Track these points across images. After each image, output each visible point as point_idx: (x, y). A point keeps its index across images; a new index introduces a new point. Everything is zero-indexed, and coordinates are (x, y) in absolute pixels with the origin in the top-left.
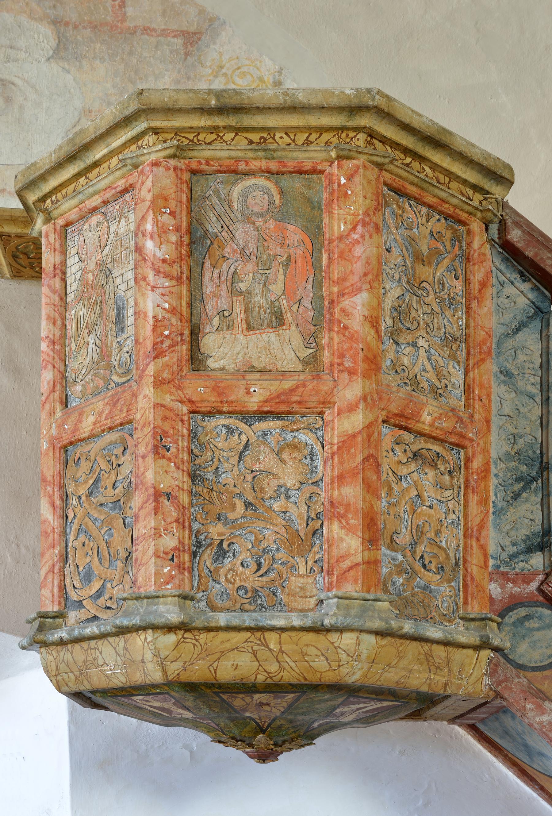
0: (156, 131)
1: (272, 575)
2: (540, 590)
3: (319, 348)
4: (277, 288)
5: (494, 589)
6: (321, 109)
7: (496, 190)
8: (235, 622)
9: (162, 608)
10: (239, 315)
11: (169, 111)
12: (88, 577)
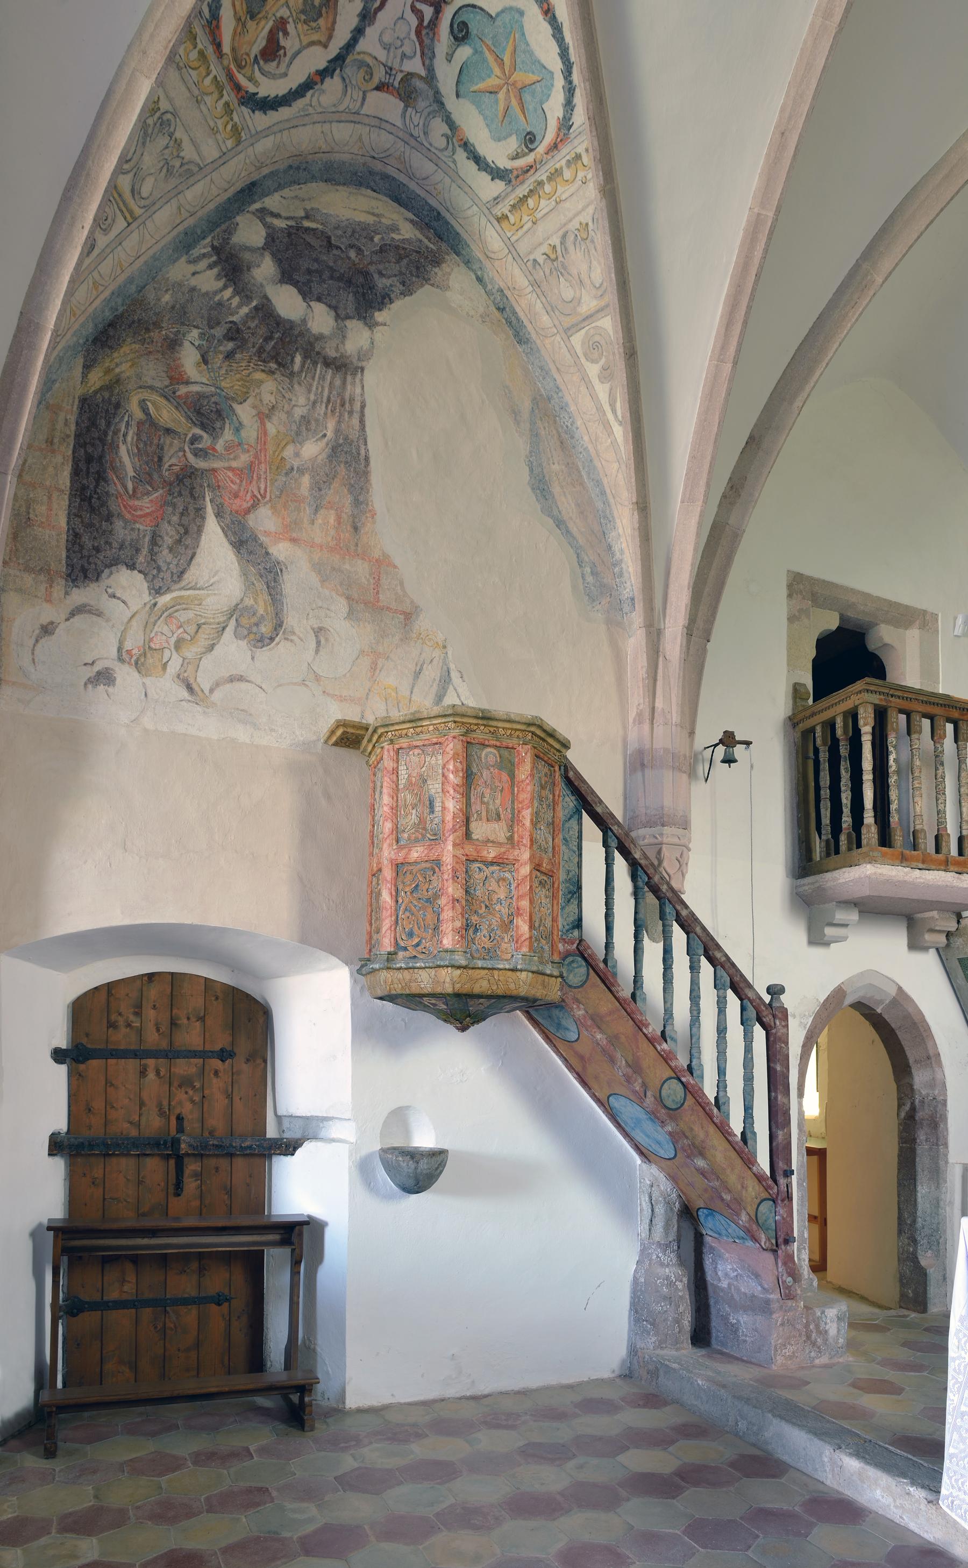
0: (455, 722)
1: (495, 942)
2: (577, 948)
3: (513, 833)
4: (498, 802)
5: (561, 947)
6: (519, 723)
7: (563, 750)
8: (485, 966)
9: (457, 957)
10: (484, 814)
11: (463, 716)
12: (411, 935)
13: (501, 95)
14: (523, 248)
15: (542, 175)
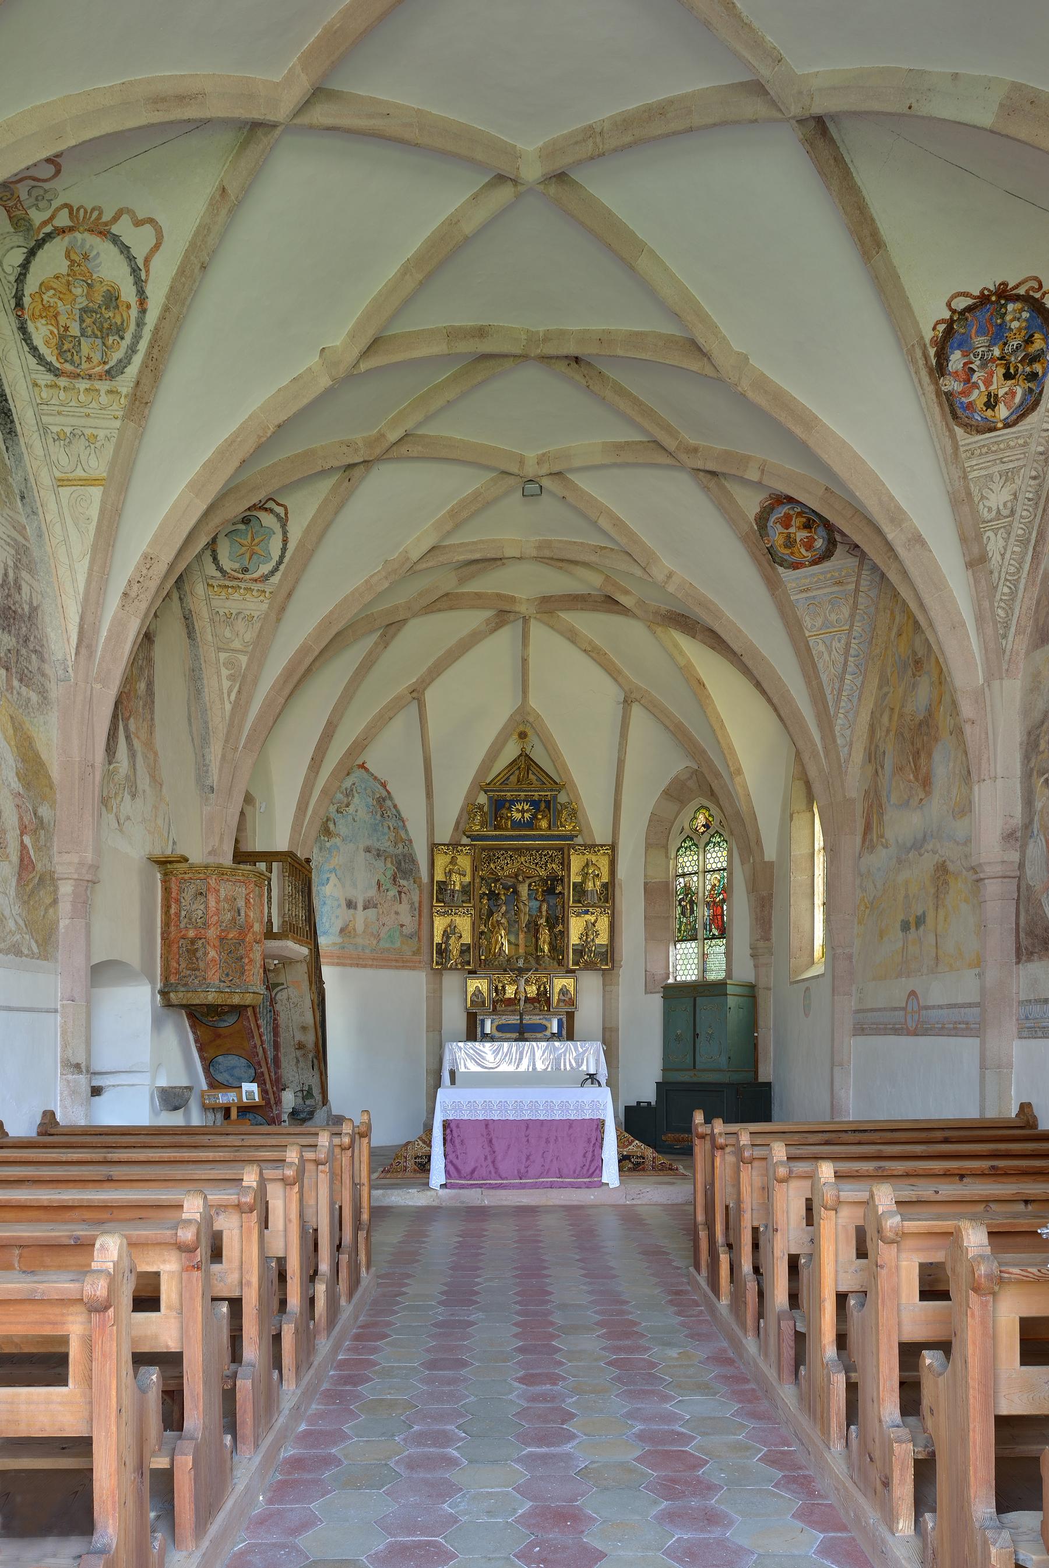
13: (244, 549)
14: (214, 603)
15: (243, 585)
